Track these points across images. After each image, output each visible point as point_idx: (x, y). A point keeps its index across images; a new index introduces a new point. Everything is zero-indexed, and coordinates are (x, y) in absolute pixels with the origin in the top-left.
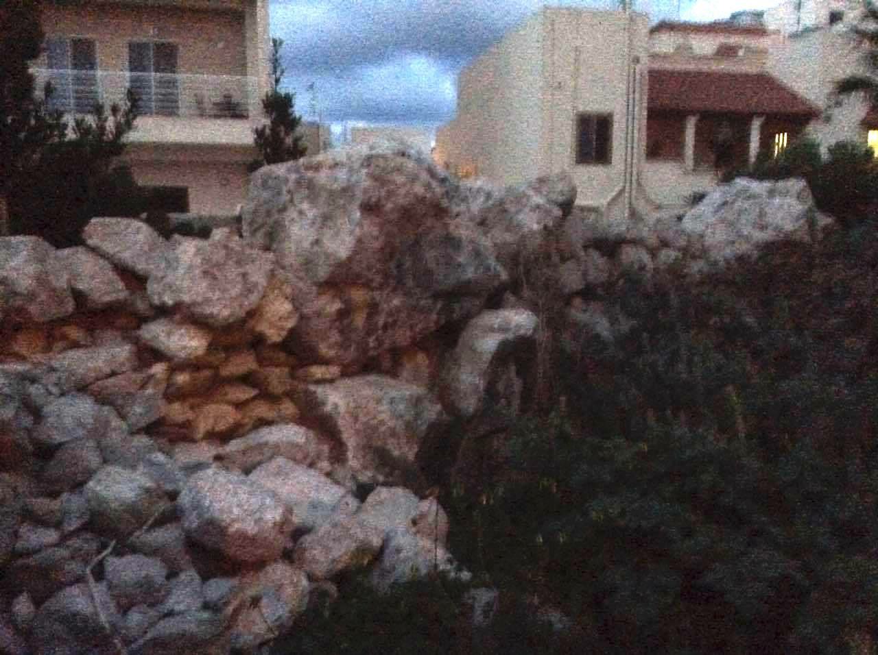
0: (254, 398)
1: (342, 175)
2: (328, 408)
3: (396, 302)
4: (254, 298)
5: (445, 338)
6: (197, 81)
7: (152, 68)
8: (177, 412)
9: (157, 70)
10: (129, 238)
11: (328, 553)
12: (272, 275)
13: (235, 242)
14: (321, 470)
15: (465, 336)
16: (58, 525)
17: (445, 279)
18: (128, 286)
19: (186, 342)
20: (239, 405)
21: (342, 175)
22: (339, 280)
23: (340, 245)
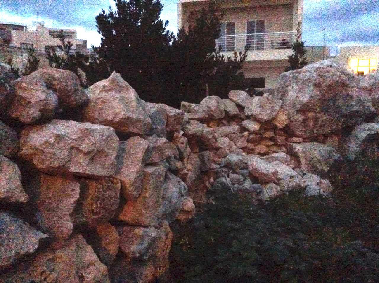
0: (273, 145)
1: (308, 74)
2: (297, 150)
3: (325, 118)
4: (274, 114)
5: (346, 132)
6: (273, 34)
7: (255, 31)
8: (251, 146)
9: (257, 32)
10: (240, 96)
11: (286, 185)
12: (282, 107)
13: (270, 97)
14: (291, 167)
15: (354, 132)
16: (219, 164)
17: (345, 110)
18: (239, 111)
19: (253, 126)
20: (268, 146)
21: (308, 74)
22: (304, 109)
23: (305, 98)
